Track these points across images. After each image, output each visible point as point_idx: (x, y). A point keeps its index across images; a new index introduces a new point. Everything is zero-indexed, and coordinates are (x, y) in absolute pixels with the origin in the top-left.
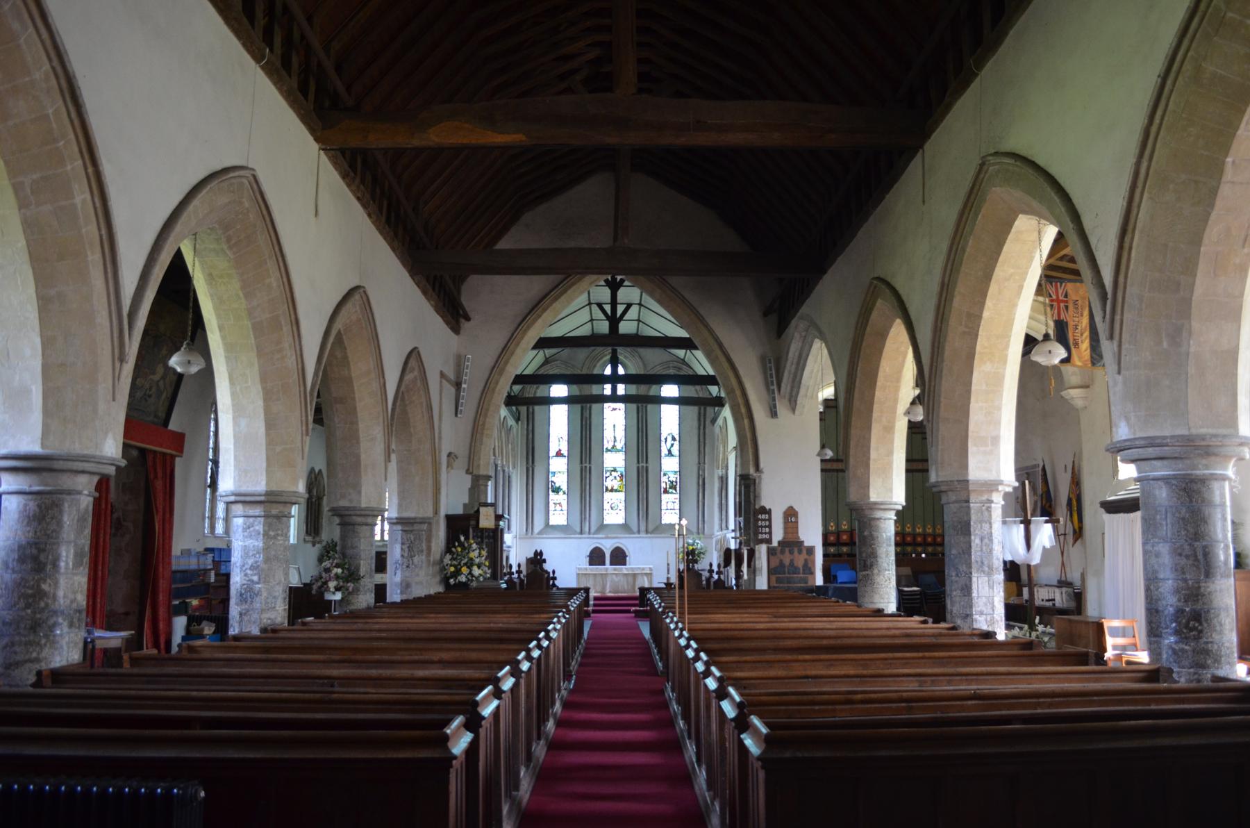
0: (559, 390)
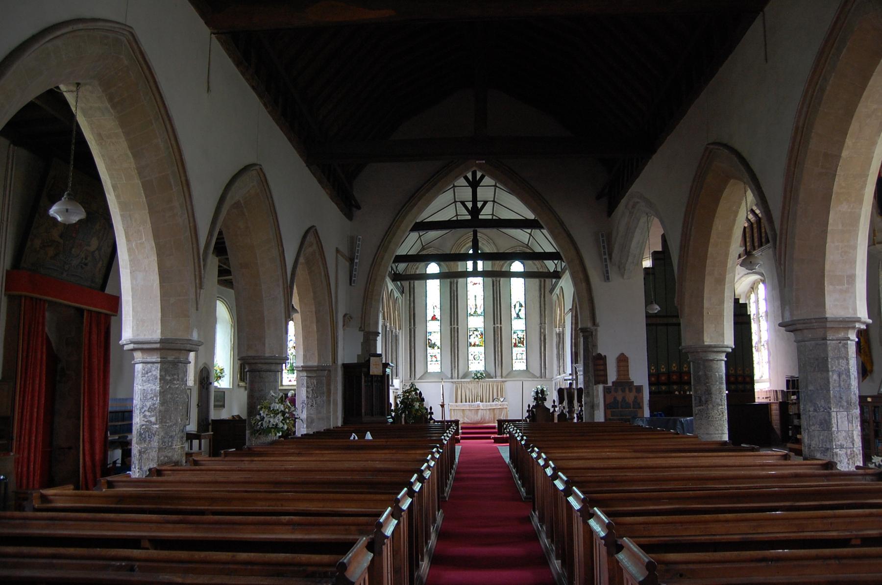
0: (433, 268)
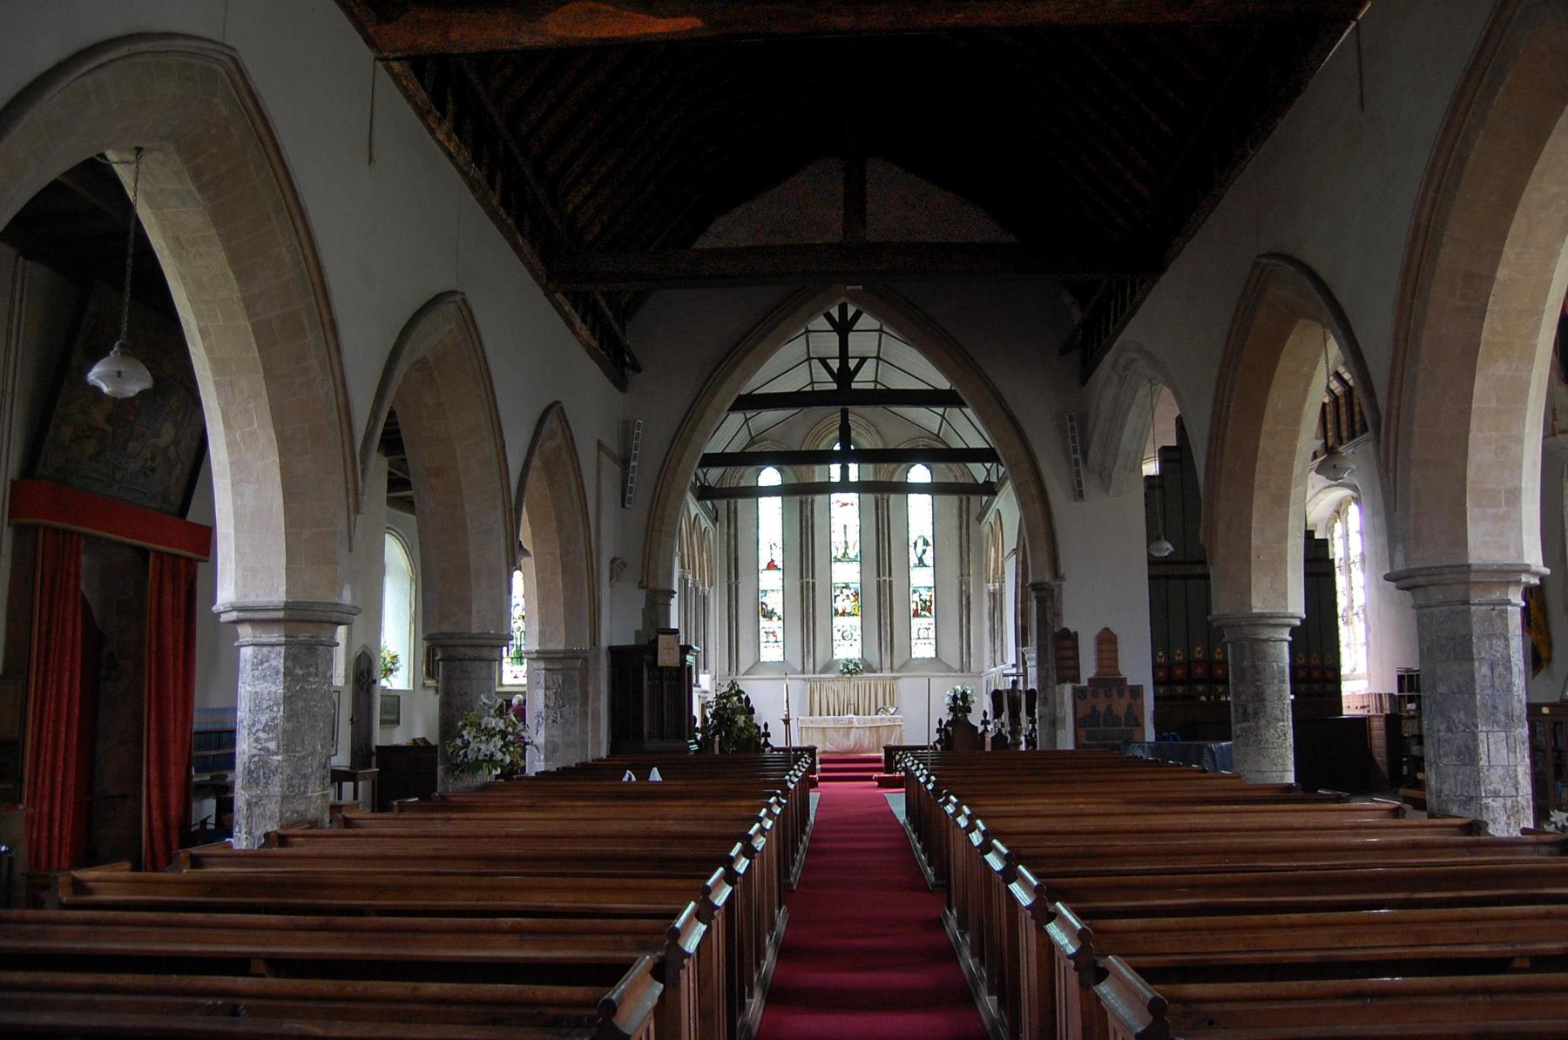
0: (770, 476)
